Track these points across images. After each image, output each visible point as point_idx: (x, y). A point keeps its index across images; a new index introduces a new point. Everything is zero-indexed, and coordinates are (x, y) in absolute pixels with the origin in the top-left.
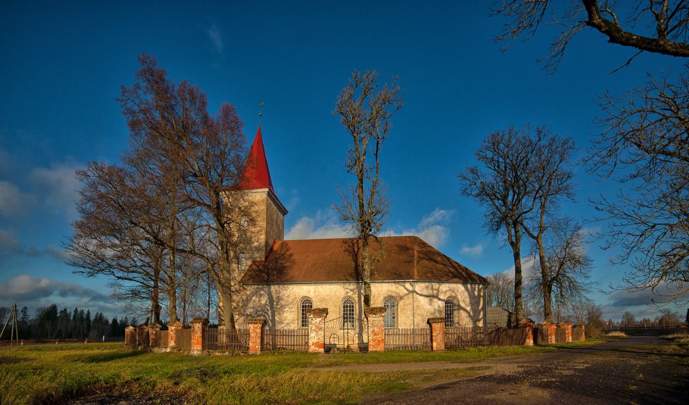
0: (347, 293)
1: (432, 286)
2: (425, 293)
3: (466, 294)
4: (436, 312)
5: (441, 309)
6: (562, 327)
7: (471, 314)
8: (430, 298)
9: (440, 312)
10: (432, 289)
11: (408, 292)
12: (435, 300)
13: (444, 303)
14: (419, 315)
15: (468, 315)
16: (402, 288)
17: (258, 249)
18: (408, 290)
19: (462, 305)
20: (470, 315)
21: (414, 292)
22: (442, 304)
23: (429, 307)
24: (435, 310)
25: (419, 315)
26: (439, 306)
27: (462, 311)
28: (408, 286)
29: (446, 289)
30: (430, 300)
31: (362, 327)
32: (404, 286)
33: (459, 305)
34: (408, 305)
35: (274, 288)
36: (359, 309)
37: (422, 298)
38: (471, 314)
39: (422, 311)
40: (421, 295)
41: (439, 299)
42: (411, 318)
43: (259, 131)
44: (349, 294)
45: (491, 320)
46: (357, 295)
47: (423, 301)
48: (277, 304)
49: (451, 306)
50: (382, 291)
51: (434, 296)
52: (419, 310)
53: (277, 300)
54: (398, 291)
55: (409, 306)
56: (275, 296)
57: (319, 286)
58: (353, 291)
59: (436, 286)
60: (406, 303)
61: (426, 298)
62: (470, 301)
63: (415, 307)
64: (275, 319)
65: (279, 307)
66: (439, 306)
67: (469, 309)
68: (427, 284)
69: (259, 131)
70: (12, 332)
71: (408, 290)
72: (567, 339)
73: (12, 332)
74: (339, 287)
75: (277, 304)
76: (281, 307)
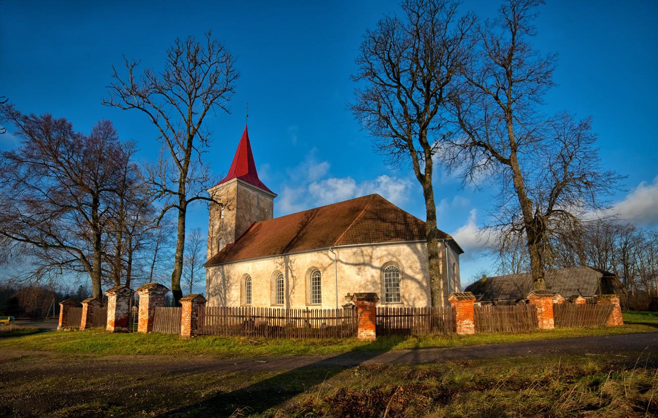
0: (277, 267)
1: (362, 252)
2: (352, 261)
3: (415, 257)
4: (368, 283)
5: (376, 279)
6: (532, 303)
7: (425, 284)
8: (359, 267)
9: (374, 283)
10: (363, 255)
11: (332, 261)
12: (367, 268)
13: (379, 271)
14: (343, 288)
15: (417, 285)
16: (325, 257)
17: (230, 233)
18: (331, 259)
19: (409, 272)
20: (421, 286)
21: (337, 260)
22: (376, 273)
23: (358, 278)
24: (367, 281)
25: (343, 288)
26: (372, 276)
27: (409, 282)
28: (330, 253)
29: (382, 253)
30: (359, 269)
31: (289, 303)
32: (327, 255)
33: (403, 273)
34: (330, 276)
35: (226, 267)
36: (286, 284)
37: (347, 266)
38: (425, 284)
39: (348, 283)
40: (346, 264)
41: (373, 267)
42: (334, 292)
43: (246, 144)
44: (278, 269)
45: (572, 286)
46: (285, 269)
47: (350, 271)
48: (228, 283)
49: (392, 275)
50: (305, 262)
51: (364, 264)
52: (343, 282)
53: (227, 279)
54: (320, 261)
55: (332, 278)
56: (226, 275)
57: (255, 263)
58: (281, 265)
59: (367, 250)
60: (329, 274)
61: (353, 267)
62: (422, 266)
63: (339, 279)
64: (225, 297)
65: (228, 285)
66: (372, 276)
67: (419, 277)
68: (355, 250)
69: (246, 144)
70: (61, 314)
71: (331, 259)
72: (540, 323)
73: (61, 314)
74: (270, 261)
75: (228, 283)
76: (230, 285)
